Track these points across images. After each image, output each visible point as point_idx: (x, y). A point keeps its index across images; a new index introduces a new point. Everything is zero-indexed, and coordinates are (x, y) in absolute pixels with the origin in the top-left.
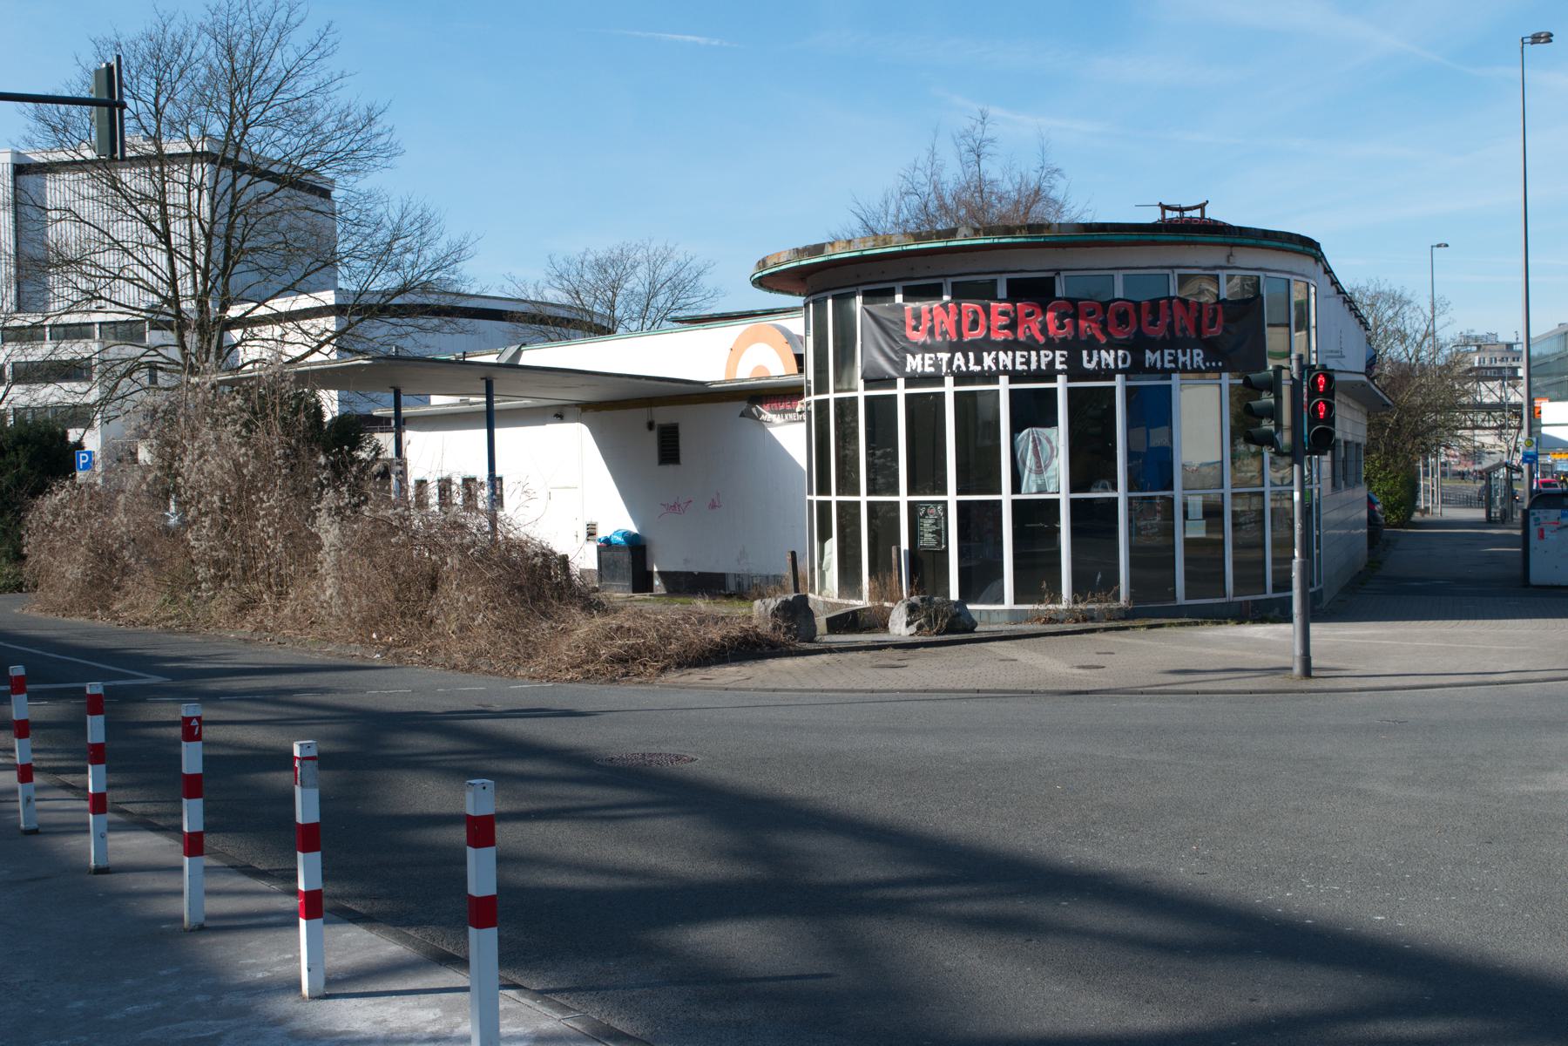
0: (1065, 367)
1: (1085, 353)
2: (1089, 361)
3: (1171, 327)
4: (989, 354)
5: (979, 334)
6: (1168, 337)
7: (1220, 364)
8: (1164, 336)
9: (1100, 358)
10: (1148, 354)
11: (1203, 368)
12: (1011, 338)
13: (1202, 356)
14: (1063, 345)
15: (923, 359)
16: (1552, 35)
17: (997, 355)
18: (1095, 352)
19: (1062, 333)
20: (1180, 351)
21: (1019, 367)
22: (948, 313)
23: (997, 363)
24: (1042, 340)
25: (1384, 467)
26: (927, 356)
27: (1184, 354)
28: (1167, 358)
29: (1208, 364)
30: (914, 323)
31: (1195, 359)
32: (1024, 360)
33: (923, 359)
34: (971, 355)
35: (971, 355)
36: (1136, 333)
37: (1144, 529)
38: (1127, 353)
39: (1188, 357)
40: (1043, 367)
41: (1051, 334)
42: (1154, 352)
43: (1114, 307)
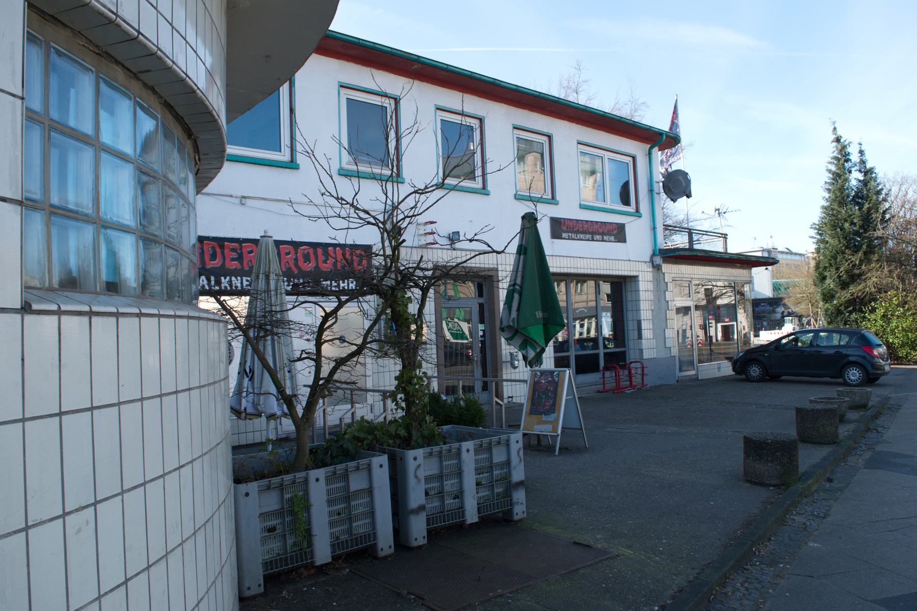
4: (225, 278)
5: (217, 263)
12: (239, 267)
15: (242, 280)
17: (230, 279)
20: (341, 281)
23: (231, 285)
25: (904, 303)
26: (244, 278)
27: (344, 282)
32: (248, 283)
33: (242, 280)
34: (213, 278)
35: (213, 278)
36: (315, 268)
37: (849, 315)
39: (346, 284)
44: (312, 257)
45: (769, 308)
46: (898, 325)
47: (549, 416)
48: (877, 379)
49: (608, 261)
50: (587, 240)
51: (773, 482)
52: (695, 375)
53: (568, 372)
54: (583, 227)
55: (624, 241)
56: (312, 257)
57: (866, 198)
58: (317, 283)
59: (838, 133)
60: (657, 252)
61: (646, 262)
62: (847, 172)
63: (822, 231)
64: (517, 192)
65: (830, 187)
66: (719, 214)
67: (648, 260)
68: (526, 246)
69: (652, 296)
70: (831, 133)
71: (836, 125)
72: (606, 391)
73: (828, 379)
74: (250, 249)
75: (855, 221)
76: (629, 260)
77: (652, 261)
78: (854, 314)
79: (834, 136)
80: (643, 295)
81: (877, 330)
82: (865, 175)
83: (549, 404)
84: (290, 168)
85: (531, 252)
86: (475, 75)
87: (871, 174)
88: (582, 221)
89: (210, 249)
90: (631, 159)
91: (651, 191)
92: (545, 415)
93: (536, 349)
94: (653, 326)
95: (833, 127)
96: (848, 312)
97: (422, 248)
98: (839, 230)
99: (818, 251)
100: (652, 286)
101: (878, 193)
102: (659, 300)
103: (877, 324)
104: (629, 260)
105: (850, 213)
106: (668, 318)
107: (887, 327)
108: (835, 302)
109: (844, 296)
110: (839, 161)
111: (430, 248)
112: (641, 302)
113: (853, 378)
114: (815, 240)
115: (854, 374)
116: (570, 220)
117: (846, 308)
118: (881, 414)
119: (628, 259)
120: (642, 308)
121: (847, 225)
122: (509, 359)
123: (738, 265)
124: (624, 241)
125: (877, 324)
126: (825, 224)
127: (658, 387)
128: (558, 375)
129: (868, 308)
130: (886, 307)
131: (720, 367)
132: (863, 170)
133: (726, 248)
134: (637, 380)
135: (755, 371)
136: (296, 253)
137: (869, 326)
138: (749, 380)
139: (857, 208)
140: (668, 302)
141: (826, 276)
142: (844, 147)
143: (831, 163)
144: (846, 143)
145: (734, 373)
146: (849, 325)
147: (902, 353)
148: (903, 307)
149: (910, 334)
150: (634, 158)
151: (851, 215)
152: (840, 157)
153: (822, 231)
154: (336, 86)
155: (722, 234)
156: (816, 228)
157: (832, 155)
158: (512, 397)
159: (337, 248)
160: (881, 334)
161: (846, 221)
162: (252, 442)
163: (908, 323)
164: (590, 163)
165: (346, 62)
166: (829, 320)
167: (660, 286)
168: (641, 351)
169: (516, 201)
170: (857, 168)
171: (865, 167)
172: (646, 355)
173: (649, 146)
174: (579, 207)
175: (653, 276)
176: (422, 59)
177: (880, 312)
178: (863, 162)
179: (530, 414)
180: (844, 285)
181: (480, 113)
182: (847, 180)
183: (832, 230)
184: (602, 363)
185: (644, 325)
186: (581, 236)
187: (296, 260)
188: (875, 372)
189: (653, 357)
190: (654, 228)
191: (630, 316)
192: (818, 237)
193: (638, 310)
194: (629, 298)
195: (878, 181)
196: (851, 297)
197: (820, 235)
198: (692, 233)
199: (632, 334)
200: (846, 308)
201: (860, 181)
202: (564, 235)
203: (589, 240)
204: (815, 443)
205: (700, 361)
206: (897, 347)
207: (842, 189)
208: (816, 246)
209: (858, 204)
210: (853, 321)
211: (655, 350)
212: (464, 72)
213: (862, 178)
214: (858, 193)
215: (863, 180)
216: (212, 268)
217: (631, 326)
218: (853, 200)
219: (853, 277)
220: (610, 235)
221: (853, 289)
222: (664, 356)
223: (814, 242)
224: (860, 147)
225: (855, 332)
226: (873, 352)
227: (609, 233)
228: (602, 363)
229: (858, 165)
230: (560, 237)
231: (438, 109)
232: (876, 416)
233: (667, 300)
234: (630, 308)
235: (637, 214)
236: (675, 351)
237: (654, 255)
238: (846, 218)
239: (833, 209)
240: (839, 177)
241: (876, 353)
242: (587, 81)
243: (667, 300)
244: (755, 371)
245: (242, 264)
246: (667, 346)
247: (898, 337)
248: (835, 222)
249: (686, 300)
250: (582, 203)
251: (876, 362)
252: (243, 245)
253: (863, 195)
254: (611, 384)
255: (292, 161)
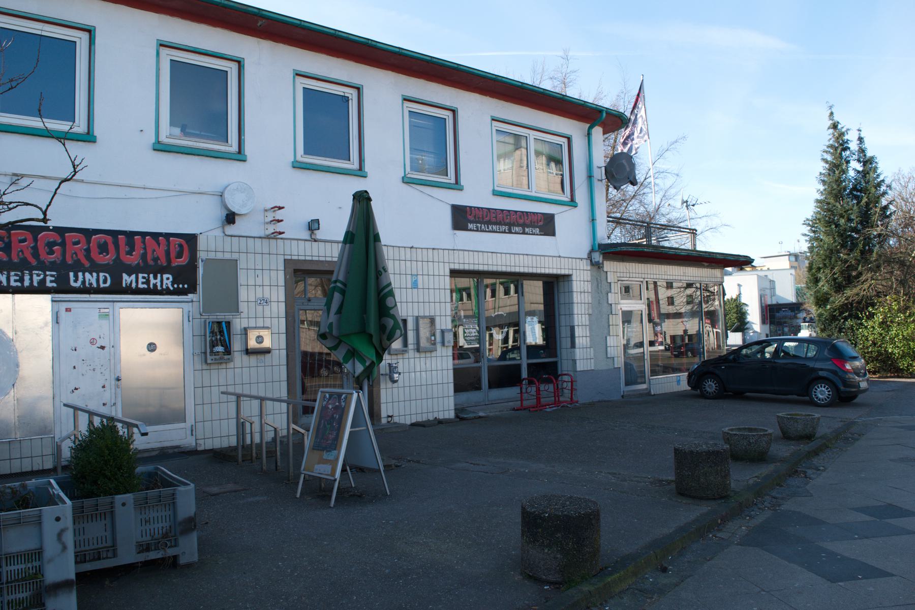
0: (55, 285)
1: (71, 274)
2: (76, 281)
3: (144, 257)
6: (142, 265)
7: (186, 286)
8: (139, 263)
9: (84, 278)
10: (125, 276)
11: (172, 288)
13: (171, 279)
14: (53, 266)
16: (900, 168)
18: (80, 274)
19: (52, 258)
20: (151, 276)
21: (141, 286)
22: (159, 244)
24: (88, 265)
27: (155, 278)
28: (141, 280)
29: (176, 286)
30: (127, 249)
31: (165, 281)
32: (145, 280)
36: (115, 260)
37: (844, 322)
38: (107, 275)
40: (35, 284)
41: (42, 258)
42: (130, 275)
43: (95, 239)
44: (111, 247)
45: (790, 313)
46: (898, 333)
47: (330, 453)
48: (855, 397)
49: (530, 257)
50: (502, 232)
51: (551, 578)
52: (646, 389)
53: (355, 395)
54: (496, 217)
55: (553, 234)
56: (111, 247)
57: (864, 190)
58: (117, 280)
59: (835, 118)
60: (597, 247)
61: (582, 259)
62: (844, 162)
63: (816, 227)
64: (405, 175)
65: (825, 179)
66: (687, 206)
67: (586, 256)
68: (354, 232)
69: (590, 298)
70: (828, 118)
71: (833, 110)
72: (525, 409)
73: (795, 397)
74: (23, 238)
75: (852, 217)
76: (559, 257)
77: (590, 257)
78: (849, 320)
79: (831, 122)
80: (576, 298)
81: (874, 339)
82: (864, 165)
83: (333, 436)
84: (84, 141)
85: (360, 239)
86: (340, 34)
87: (871, 163)
88: (496, 210)
89: (177, 246)
90: (565, 140)
91: (590, 177)
92: (328, 451)
93: (365, 362)
94: (590, 333)
95: (830, 111)
96: (842, 318)
97: (269, 238)
98: (833, 226)
99: (811, 249)
100: (590, 286)
101: (879, 185)
102: (599, 303)
103: (875, 332)
104: (559, 257)
105: (847, 208)
106: (611, 323)
107: (886, 335)
108: (828, 307)
109: (838, 300)
110: (836, 150)
111: (282, 239)
112: (575, 305)
113: (820, 396)
114: (807, 238)
115: (822, 392)
116: (478, 208)
117: (841, 313)
118: (828, 447)
119: (557, 255)
120: (575, 312)
121: (842, 221)
122: (388, 372)
123: (706, 264)
124: (553, 234)
125: (875, 332)
126: (819, 219)
127: (592, 404)
128: (346, 398)
129: (865, 314)
130: (885, 312)
131: (679, 380)
132: (862, 160)
133: (695, 245)
134: (566, 396)
135: (711, 386)
136: (89, 242)
137: (866, 334)
138: (704, 396)
139: (855, 202)
140: (611, 305)
141: (820, 278)
142: (842, 134)
143: (826, 152)
144: (843, 130)
145: (690, 388)
146: (843, 332)
147: (903, 364)
148: (904, 313)
149: (911, 343)
150: (569, 139)
151: (848, 211)
152: (837, 145)
153: (816, 227)
154: (154, 45)
155: (690, 229)
156: (809, 224)
157: (827, 143)
158: (391, 417)
159: (147, 237)
160: (879, 343)
161: (842, 216)
162: (19, 471)
163: (909, 331)
164: (514, 145)
165: (169, 17)
166: (823, 327)
167: (600, 286)
168: (574, 361)
169: (405, 186)
170: (855, 157)
171: (865, 155)
172: (580, 367)
173: (589, 125)
174: (491, 193)
175: (592, 276)
176: (264, 13)
177: (879, 318)
178: (862, 151)
179: (313, 449)
180: (839, 288)
181: (356, 81)
182: (844, 172)
183: (826, 227)
184: (524, 374)
185: (578, 332)
186: (494, 227)
187: (88, 251)
188: (848, 389)
189: (589, 369)
190: (593, 220)
191: (563, 321)
192: (812, 234)
193: (571, 314)
194: (562, 301)
195: (879, 171)
196: (846, 302)
197: (814, 232)
198: (650, 227)
199: (565, 342)
200: (841, 313)
201: (859, 172)
202: (470, 226)
203: (504, 232)
204: (694, 498)
205: (654, 372)
206: (897, 358)
207: (839, 181)
208: (809, 245)
209: (856, 197)
210: (849, 328)
211: (592, 361)
212: (325, 30)
213: (861, 169)
214: (856, 185)
215: (863, 171)
216: (177, 266)
217: (564, 332)
218: (851, 192)
219: (848, 279)
220: (535, 227)
221: (849, 292)
222: (605, 368)
223: (806, 240)
224: (860, 134)
225: (825, 342)
226: (845, 366)
227: (533, 225)
228: (524, 374)
229: (856, 154)
230: (465, 229)
231: (406, 99)
232: (816, 453)
233: (610, 302)
234: (562, 312)
235: (572, 203)
236: (620, 362)
237: (592, 251)
238: (842, 214)
239: (828, 204)
240: (836, 167)
241: (848, 367)
242: (575, 72)
243: (610, 302)
244: (711, 386)
245: (9, 255)
246: (609, 356)
247: (898, 347)
248: (830, 218)
249: (637, 304)
250: (496, 188)
251: (849, 378)
252: (12, 232)
253: (861, 188)
254: (530, 402)
255: (239, 152)
